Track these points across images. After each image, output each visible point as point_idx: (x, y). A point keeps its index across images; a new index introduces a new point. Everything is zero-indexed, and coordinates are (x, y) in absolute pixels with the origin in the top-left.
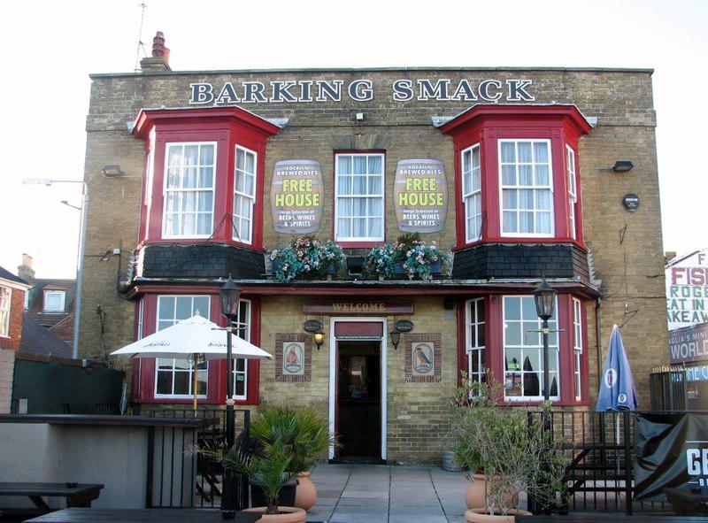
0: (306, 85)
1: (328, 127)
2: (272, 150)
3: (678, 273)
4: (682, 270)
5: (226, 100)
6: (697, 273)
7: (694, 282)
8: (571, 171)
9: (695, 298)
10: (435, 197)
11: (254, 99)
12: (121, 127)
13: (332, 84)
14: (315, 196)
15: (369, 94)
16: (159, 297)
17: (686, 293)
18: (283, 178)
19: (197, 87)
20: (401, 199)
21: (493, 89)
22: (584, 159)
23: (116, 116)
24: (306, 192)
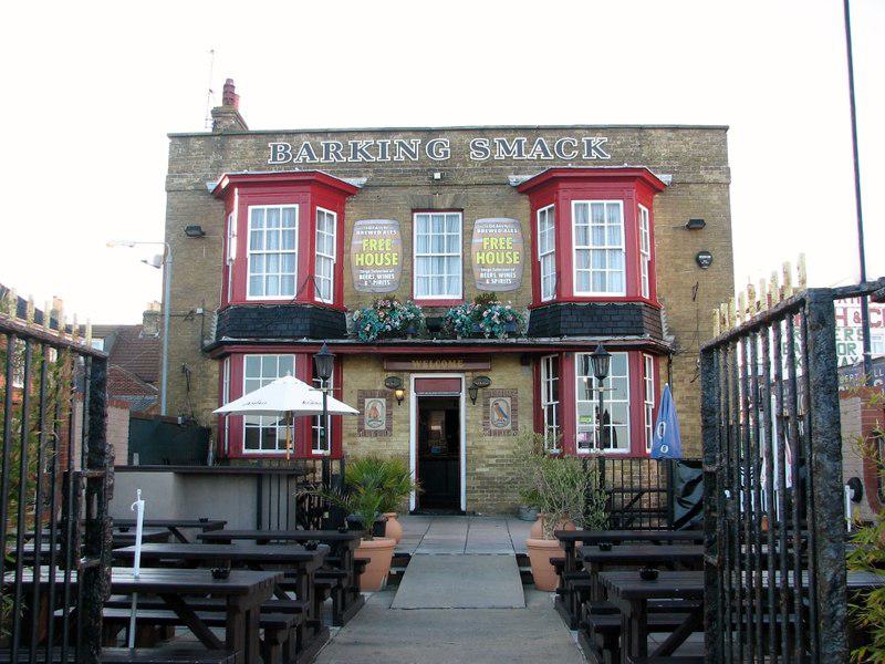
0: (384, 144)
1: (406, 186)
5: (305, 159)
10: (511, 256)
11: (333, 158)
12: (200, 187)
15: (446, 152)
16: (245, 356)
18: (363, 237)
19: (275, 147)
20: (358, 259)
22: (659, 217)
24: (385, 252)
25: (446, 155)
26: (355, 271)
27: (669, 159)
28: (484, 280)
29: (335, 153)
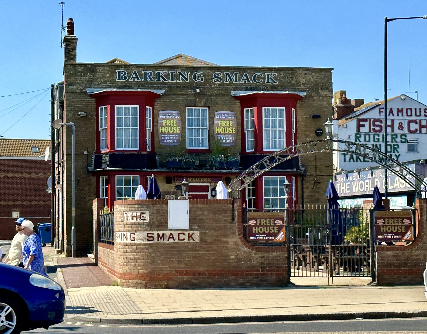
0: (172, 74)
1: (183, 95)
2: (157, 105)
3: (362, 123)
4: (366, 120)
5: (134, 79)
6: (377, 123)
7: (374, 130)
8: (293, 120)
9: (375, 143)
10: (232, 129)
11: (148, 80)
13: (184, 73)
14: (178, 128)
15: (202, 79)
17: (367, 139)
18: (163, 119)
19: (119, 72)
20: (161, 130)
21: (259, 78)
22: (299, 112)
23: (80, 85)
25: (202, 80)
26: (160, 136)
27: (304, 84)
28: (164, 140)
29: (149, 77)
